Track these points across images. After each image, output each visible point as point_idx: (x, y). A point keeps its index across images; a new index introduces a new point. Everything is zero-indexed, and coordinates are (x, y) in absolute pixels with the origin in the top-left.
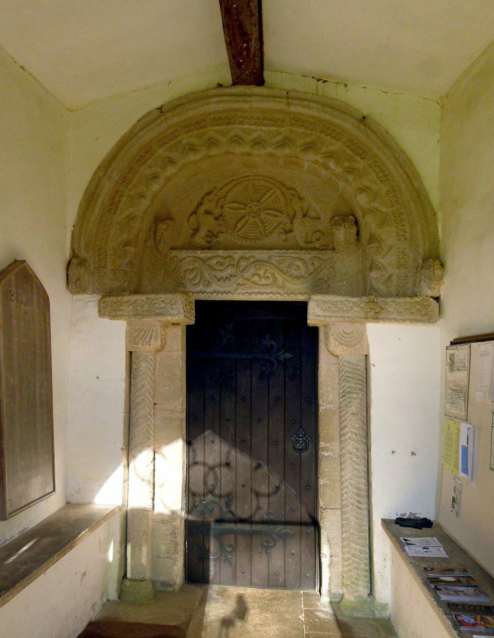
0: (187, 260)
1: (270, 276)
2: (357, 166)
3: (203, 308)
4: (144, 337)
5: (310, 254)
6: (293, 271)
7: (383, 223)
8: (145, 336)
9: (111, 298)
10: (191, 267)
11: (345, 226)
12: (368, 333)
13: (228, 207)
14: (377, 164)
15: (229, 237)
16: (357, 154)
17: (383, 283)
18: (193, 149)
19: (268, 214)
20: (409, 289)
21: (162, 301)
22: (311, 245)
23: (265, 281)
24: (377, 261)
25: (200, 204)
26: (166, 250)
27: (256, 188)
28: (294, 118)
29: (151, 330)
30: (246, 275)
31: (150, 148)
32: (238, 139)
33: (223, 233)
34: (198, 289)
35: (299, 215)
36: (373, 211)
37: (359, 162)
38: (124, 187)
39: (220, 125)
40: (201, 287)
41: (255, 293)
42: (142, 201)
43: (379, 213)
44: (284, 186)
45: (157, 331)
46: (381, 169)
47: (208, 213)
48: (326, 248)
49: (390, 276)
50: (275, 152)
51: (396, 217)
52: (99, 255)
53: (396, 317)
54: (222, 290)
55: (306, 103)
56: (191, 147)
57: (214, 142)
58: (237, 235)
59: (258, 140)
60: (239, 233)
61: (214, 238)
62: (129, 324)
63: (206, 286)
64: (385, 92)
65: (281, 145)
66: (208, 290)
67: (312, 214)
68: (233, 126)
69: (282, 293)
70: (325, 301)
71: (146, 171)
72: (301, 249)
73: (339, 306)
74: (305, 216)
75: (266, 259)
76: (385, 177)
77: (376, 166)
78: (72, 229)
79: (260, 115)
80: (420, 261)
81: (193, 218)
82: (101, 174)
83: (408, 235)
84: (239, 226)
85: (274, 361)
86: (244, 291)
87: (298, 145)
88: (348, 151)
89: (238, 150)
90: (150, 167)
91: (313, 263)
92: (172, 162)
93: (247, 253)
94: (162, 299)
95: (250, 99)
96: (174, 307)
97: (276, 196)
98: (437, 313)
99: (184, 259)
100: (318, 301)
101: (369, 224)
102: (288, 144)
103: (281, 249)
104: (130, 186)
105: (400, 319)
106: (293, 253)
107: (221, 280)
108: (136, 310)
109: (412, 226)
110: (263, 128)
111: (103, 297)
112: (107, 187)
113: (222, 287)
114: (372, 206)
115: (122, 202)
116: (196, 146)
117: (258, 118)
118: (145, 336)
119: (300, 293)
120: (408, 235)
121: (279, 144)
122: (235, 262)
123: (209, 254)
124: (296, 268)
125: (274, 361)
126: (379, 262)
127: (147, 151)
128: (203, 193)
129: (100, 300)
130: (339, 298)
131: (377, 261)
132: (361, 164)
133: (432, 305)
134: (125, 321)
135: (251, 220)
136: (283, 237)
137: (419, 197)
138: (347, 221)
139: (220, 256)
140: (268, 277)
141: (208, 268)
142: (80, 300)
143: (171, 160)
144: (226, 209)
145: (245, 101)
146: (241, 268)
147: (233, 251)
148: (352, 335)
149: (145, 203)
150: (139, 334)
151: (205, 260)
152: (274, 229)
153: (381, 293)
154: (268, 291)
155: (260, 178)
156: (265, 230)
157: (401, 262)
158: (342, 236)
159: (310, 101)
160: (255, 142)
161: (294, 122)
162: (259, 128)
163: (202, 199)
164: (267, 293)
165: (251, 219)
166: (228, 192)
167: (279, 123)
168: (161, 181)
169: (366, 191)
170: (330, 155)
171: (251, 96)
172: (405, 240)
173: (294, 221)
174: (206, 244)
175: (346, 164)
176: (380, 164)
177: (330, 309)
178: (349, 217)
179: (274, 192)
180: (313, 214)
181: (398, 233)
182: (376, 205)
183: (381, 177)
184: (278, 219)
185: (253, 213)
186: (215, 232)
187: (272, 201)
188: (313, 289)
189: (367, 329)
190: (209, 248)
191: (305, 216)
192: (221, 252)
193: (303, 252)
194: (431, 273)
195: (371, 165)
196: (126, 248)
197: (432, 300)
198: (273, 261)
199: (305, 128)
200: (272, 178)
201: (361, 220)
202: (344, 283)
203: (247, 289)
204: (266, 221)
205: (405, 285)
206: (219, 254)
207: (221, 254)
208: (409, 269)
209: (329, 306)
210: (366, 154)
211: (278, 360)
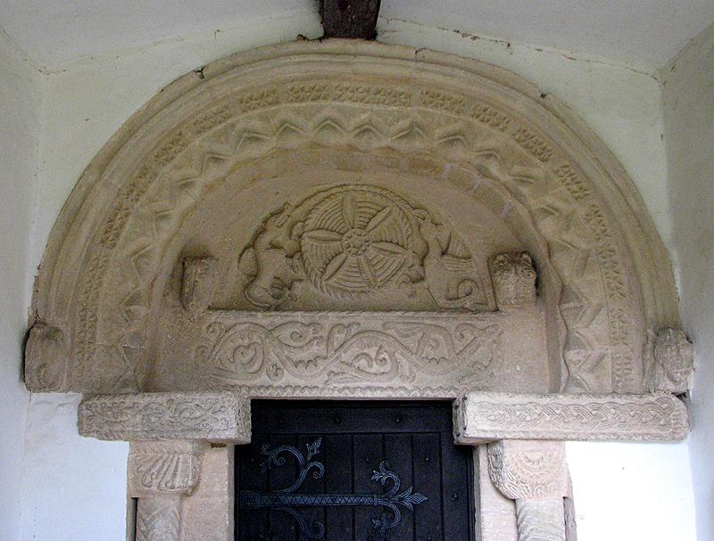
0: (238, 328)
1: (387, 357)
2: (535, 172)
3: (265, 412)
4: (162, 472)
5: (456, 319)
6: (428, 349)
7: (584, 265)
9: (102, 400)
13: (309, 237)
15: (312, 288)
17: (592, 370)
18: (253, 137)
19: (381, 249)
22: (458, 304)
27: (360, 205)
28: (427, 93)
29: (176, 459)
30: (344, 357)
31: (180, 134)
33: (301, 280)
34: (258, 382)
35: (435, 251)
37: (537, 166)
39: (302, 100)
40: (263, 379)
42: (163, 224)
45: (185, 462)
47: (274, 246)
49: (602, 358)
50: (396, 145)
52: (82, 320)
54: (302, 383)
55: (448, 70)
58: (327, 285)
59: (367, 127)
60: (330, 282)
62: (135, 450)
63: (272, 374)
64: (571, 58)
65: (404, 136)
67: (456, 249)
68: (323, 102)
71: (169, 173)
72: (441, 310)
73: (518, 413)
74: (443, 253)
75: (380, 329)
77: (566, 173)
78: (35, 272)
79: (371, 86)
81: (249, 254)
82: (92, 178)
84: (330, 269)
85: (394, 507)
86: (342, 385)
87: (435, 137)
88: (519, 147)
89: (333, 139)
90: (178, 168)
92: (216, 159)
93: (347, 318)
95: (356, 60)
96: (219, 416)
97: (394, 219)
98: (684, 422)
100: (481, 404)
101: (564, 267)
102: (419, 133)
103: (407, 311)
104: (143, 199)
106: (427, 318)
107: (300, 365)
108: (149, 420)
110: (375, 107)
111: (88, 397)
112: (101, 201)
113: (301, 377)
114: (564, 238)
115: (127, 226)
116: (259, 134)
118: (164, 470)
120: (625, 289)
121: (403, 133)
123: (276, 318)
125: (394, 507)
127: (173, 143)
128: (267, 213)
129: (82, 402)
130: (518, 399)
132: (539, 170)
135: (352, 260)
136: (408, 289)
137: (640, 226)
138: (519, 262)
142: (43, 402)
144: (306, 241)
145: (347, 64)
146: (335, 344)
149: (169, 226)
151: (270, 328)
157: (618, 334)
159: (454, 66)
160: (362, 129)
161: (427, 98)
162: (368, 106)
163: (265, 222)
165: (612, 272)
166: (310, 212)
167: (404, 100)
168: (196, 191)
169: (552, 214)
170: (490, 154)
171: (355, 56)
173: (426, 262)
175: (517, 169)
178: (522, 257)
183: (577, 192)
184: (399, 259)
190: (277, 309)
191: (443, 253)
192: (299, 316)
193: (445, 315)
196: (132, 308)
197: (675, 399)
199: (447, 109)
201: (543, 260)
203: (347, 382)
206: (295, 319)
207: (300, 319)
208: (631, 346)
209: (501, 412)
211: (402, 508)
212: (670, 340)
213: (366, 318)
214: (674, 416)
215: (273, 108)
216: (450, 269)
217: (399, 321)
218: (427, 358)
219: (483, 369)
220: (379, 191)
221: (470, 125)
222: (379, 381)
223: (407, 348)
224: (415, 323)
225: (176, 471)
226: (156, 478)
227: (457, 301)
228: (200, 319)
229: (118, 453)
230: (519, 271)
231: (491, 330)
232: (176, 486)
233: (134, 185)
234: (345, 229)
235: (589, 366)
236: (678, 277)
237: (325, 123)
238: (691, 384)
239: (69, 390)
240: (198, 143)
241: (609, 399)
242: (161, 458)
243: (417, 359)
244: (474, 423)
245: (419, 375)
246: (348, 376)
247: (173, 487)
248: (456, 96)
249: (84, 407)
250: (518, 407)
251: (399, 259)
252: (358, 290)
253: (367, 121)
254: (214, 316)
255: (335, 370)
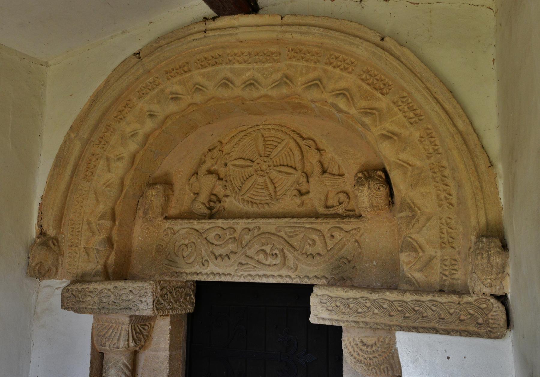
1: (278, 252)
2: (377, 105)
5: (328, 223)
8: (113, 335)
9: (76, 286)
10: (187, 242)
11: (369, 185)
12: (398, 346)
14: (405, 100)
16: (376, 89)
17: (421, 270)
19: (280, 172)
20: (459, 279)
21: (130, 291)
23: (271, 260)
24: (410, 237)
25: (202, 163)
26: (159, 219)
27: (268, 143)
28: (292, 50)
32: (227, 82)
34: (193, 270)
35: (318, 170)
36: (403, 166)
38: (101, 148)
41: (259, 276)
43: (410, 168)
44: (300, 135)
46: (412, 106)
47: (210, 172)
48: (351, 213)
49: (431, 259)
51: (435, 173)
53: (437, 325)
54: (221, 271)
55: (304, 29)
56: (174, 96)
57: (200, 87)
61: (217, 203)
62: (96, 320)
66: (204, 271)
68: (219, 67)
69: (293, 277)
70: (332, 297)
72: (317, 216)
74: (324, 172)
75: (273, 231)
76: (417, 117)
80: (473, 238)
81: (194, 179)
83: (454, 201)
87: (299, 83)
90: (129, 124)
91: (332, 236)
93: (252, 223)
94: (131, 289)
96: (143, 299)
99: (178, 231)
102: (286, 83)
105: (444, 330)
106: (307, 223)
109: (460, 186)
110: (256, 66)
111: (74, 282)
116: (179, 94)
117: (250, 54)
118: (113, 335)
119: (316, 276)
120: (454, 201)
122: (236, 235)
123: (206, 224)
124: (311, 243)
126: (412, 239)
130: (352, 293)
131: (410, 237)
133: (494, 309)
134: (92, 316)
135: (261, 180)
136: (298, 201)
139: (219, 227)
140: (276, 254)
141: (205, 242)
143: (152, 113)
145: (231, 35)
147: (234, 221)
148: (374, 348)
150: (107, 332)
152: (287, 190)
153: (416, 284)
154: (276, 274)
155: (270, 127)
156: (276, 192)
158: (366, 200)
161: (292, 54)
162: (250, 66)
164: (273, 276)
169: (391, 138)
170: (342, 93)
172: (450, 206)
174: (207, 211)
176: (410, 101)
177: (338, 309)
178: (377, 174)
179: (288, 144)
180: (335, 171)
181: (438, 196)
182: (404, 156)
184: (293, 178)
185: (261, 170)
186: (221, 195)
187: (285, 155)
188: (332, 271)
189: (397, 340)
191: (324, 172)
193: (320, 220)
194: (485, 261)
195: (397, 101)
197: (492, 300)
198: (282, 234)
200: (285, 126)
202: (375, 263)
204: (277, 180)
205: (453, 274)
206: (218, 225)
207: (220, 225)
208: (457, 250)
209: (338, 304)
210: (389, 87)
212: (482, 248)
213: (264, 224)
214: (492, 316)
215: (187, 75)
216: (328, 184)
217: (287, 225)
218: (306, 253)
219: (347, 262)
220: (280, 128)
221: (325, 71)
222: (272, 271)
223: (291, 246)
224: (298, 227)
225: (120, 334)
226: (108, 341)
227: (332, 209)
228: (159, 226)
229: (87, 320)
230: (372, 186)
231: (354, 232)
232: (121, 347)
233: (102, 138)
234: (256, 158)
235: (419, 266)
236: (501, 188)
237: (222, 82)
238: (509, 291)
239: (63, 278)
240: (143, 105)
241: (430, 297)
242: (111, 327)
243: (299, 255)
244: (316, 312)
245: (301, 266)
246: (250, 266)
247: (118, 348)
248: (315, 50)
249: (65, 291)
250: (351, 300)
251: (293, 178)
252: (263, 202)
253: (252, 77)
254: (168, 224)
255: (243, 262)
